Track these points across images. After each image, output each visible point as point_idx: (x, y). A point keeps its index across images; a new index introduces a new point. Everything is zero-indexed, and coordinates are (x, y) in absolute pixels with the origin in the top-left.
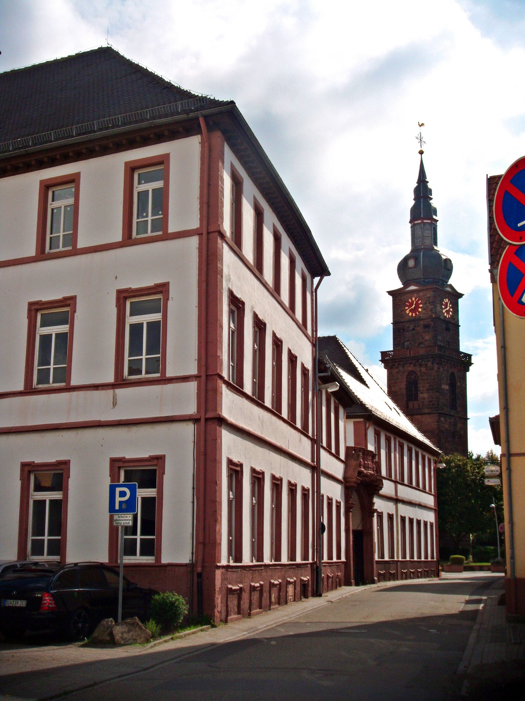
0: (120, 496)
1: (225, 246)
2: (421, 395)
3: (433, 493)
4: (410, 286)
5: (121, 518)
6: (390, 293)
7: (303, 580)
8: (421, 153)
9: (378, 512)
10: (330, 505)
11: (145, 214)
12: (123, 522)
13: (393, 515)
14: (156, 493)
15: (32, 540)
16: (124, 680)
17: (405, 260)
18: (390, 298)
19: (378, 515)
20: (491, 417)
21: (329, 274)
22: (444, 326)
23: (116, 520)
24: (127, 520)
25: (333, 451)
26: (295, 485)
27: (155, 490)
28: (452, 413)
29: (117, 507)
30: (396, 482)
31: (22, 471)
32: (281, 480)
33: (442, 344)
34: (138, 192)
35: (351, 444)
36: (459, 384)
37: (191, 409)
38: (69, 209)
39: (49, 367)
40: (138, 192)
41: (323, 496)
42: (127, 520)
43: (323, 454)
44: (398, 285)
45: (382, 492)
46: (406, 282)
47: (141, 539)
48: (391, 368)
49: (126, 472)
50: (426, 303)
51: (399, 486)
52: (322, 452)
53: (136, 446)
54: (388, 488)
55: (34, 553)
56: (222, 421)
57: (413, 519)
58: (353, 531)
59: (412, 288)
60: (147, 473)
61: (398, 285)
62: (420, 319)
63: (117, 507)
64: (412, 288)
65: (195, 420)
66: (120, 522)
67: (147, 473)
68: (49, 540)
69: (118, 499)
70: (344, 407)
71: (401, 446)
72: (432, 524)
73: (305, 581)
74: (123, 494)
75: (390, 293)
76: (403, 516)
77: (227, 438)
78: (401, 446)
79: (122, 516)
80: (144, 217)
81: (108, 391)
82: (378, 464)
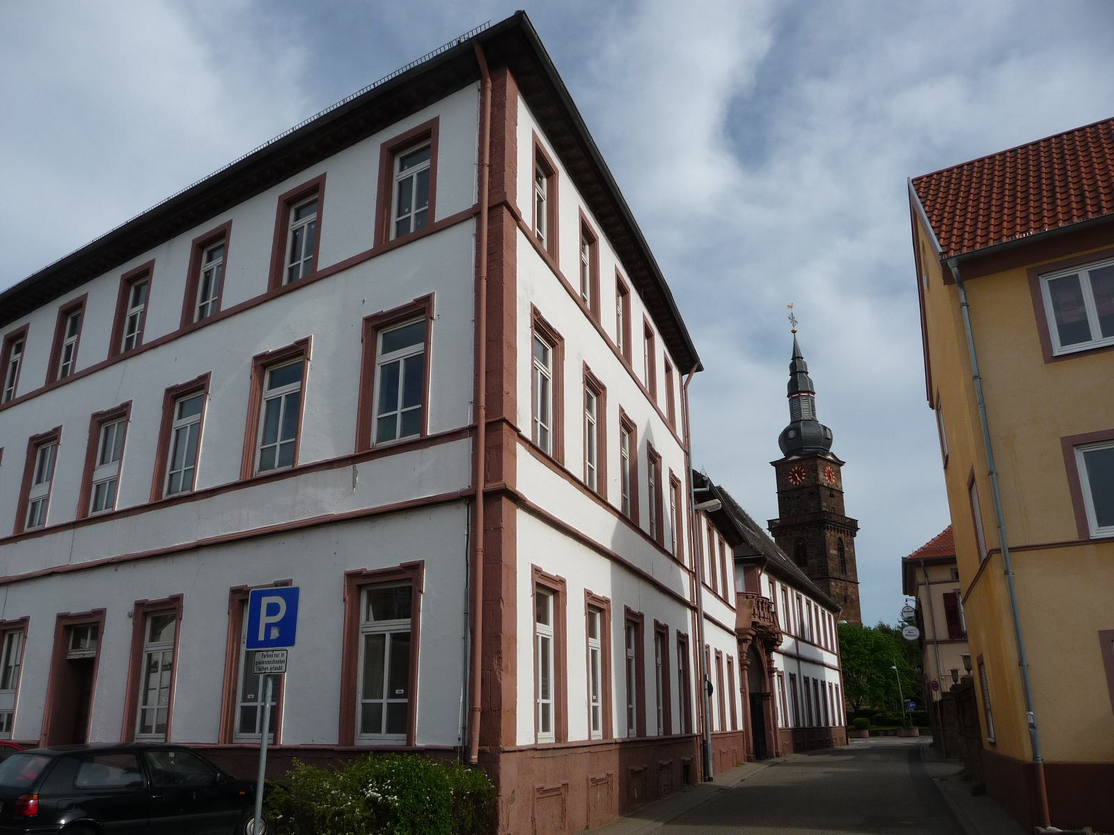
0: (268, 614)
1: (521, 238)
2: (810, 561)
4: (791, 457)
5: (266, 659)
6: (773, 464)
7: (684, 760)
8: (794, 332)
9: (778, 672)
10: (718, 659)
11: (407, 210)
12: (269, 666)
14: (410, 626)
16: (569, 825)
17: (786, 432)
19: (778, 676)
20: (906, 555)
21: (700, 369)
23: (260, 663)
24: (278, 662)
25: (720, 593)
26: (666, 628)
27: (410, 619)
29: (261, 637)
31: (231, 601)
33: (828, 510)
34: (399, 183)
35: (741, 590)
36: (847, 549)
37: (459, 482)
38: (313, 227)
39: (275, 444)
40: (399, 183)
41: (708, 647)
42: (278, 662)
43: (705, 593)
44: (780, 455)
45: (782, 647)
46: (787, 454)
47: (388, 704)
48: (779, 536)
49: (369, 593)
50: (808, 472)
52: (704, 591)
53: (379, 551)
54: (787, 643)
55: (366, 729)
56: (519, 501)
58: (750, 694)
59: (794, 457)
60: (392, 592)
61: (780, 455)
62: (804, 487)
63: (261, 637)
64: (794, 457)
65: (467, 498)
66: (265, 666)
67: (392, 592)
69: (264, 619)
70: (732, 546)
71: (799, 598)
72: (836, 685)
73: (688, 761)
74: (273, 609)
75: (773, 464)
76: (806, 676)
77: (525, 527)
78: (799, 598)
79: (270, 653)
80: (406, 213)
81: (346, 468)
82: (775, 614)
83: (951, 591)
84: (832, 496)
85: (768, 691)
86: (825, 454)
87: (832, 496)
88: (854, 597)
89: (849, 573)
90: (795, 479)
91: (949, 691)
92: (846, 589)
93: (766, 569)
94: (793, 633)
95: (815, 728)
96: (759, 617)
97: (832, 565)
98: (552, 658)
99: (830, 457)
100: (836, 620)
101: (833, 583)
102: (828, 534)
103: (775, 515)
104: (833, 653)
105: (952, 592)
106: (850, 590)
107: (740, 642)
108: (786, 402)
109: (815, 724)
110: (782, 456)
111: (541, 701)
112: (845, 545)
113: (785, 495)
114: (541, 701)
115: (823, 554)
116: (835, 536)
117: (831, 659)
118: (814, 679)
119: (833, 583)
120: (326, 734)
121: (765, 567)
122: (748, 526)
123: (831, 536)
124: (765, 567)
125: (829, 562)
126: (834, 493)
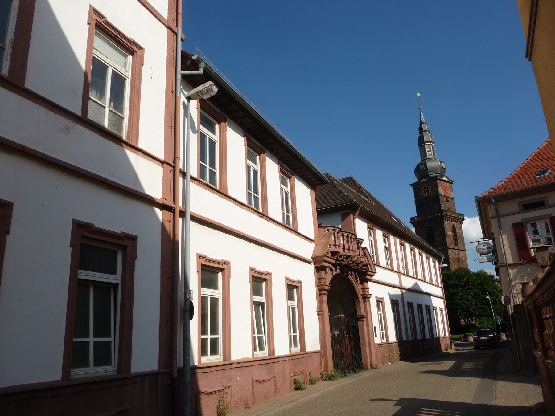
3: (440, 285)
6: (412, 185)
13: (397, 301)
15: (109, 336)
18: (412, 188)
20: (479, 195)
22: (445, 199)
26: (421, 305)
27: (79, 277)
28: (456, 247)
30: (399, 272)
32: (412, 303)
36: (458, 231)
46: (420, 179)
51: (402, 276)
57: (412, 303)
59: (424, 180)
64: (424, 180)
68: (88, 336)
75: (412, 185)
83: (519, 221)
84: (447, 201)
85: (363, 313)
86: (441, 177)
87: (447, 201)
88: (463, 259)
89: (460, 245)
90: (425, 193)
91: (521, 303)
92: (459, 254)
93: (359, 214)
94: (396, 269)
95: (419, 340)
96: (344, 249)
97: (449, 241)
98: (383, 319)
99: (445, 179)
100: (439, 264)
101: (450, 251)
102: (446, 223)
103: (414, 214)
104: (437, 286)
105: (520, 221)
106: (461, 255)
107: (319, 269)
108: (418, 148)
109: (419, 337)
110: (416, 180)
111: (292, 334)
112: (457, 229)
113: (420, 203)
114: (292, 334)
115: (443, 234)
116: (450, 224)
117: (439, 292)
118: (418, 304)
119: (450, 251)
120: (287, 353)
121: (358, 212)
122: (364, 195)
123: (448, 224)
124: (358, 212)
125: (447, 239)
126: (449, 199)
